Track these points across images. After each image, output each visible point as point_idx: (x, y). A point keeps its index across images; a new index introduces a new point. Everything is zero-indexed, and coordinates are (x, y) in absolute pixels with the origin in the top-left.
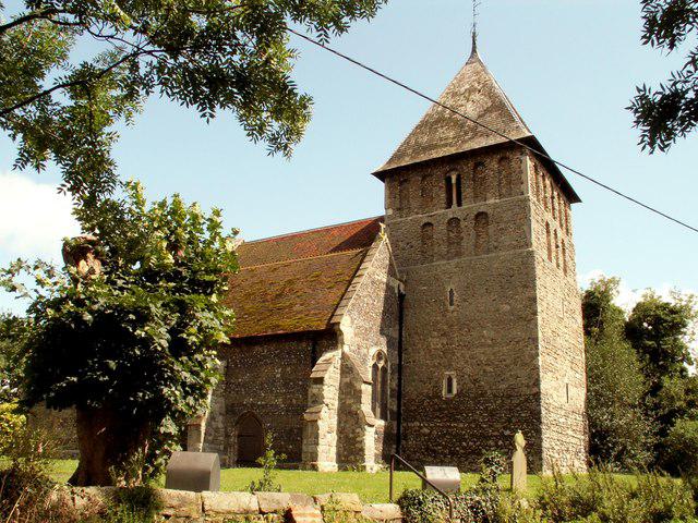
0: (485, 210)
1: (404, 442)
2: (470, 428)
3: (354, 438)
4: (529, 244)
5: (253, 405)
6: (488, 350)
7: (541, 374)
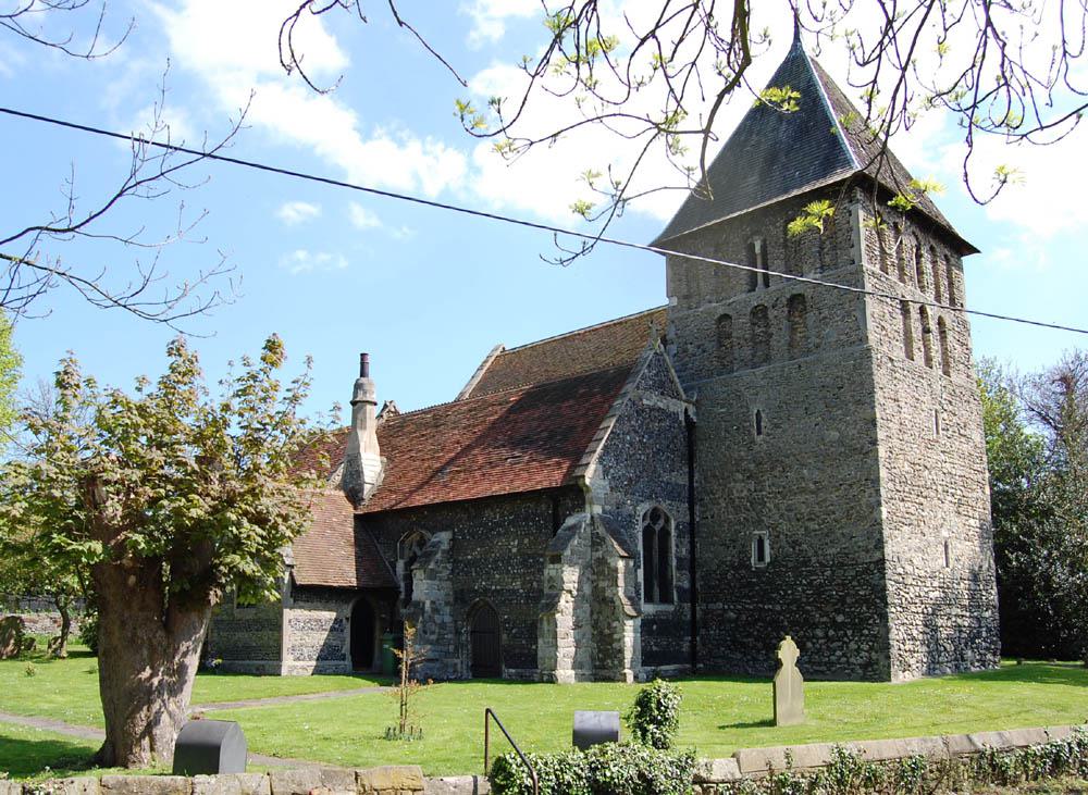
0: (802, 291)
1: (703, 631)
2: (791, 612)
3: (611, 635)
4: (864, 339)
5: (486, 590)
6: (812, 498)
7: (886, 532)
